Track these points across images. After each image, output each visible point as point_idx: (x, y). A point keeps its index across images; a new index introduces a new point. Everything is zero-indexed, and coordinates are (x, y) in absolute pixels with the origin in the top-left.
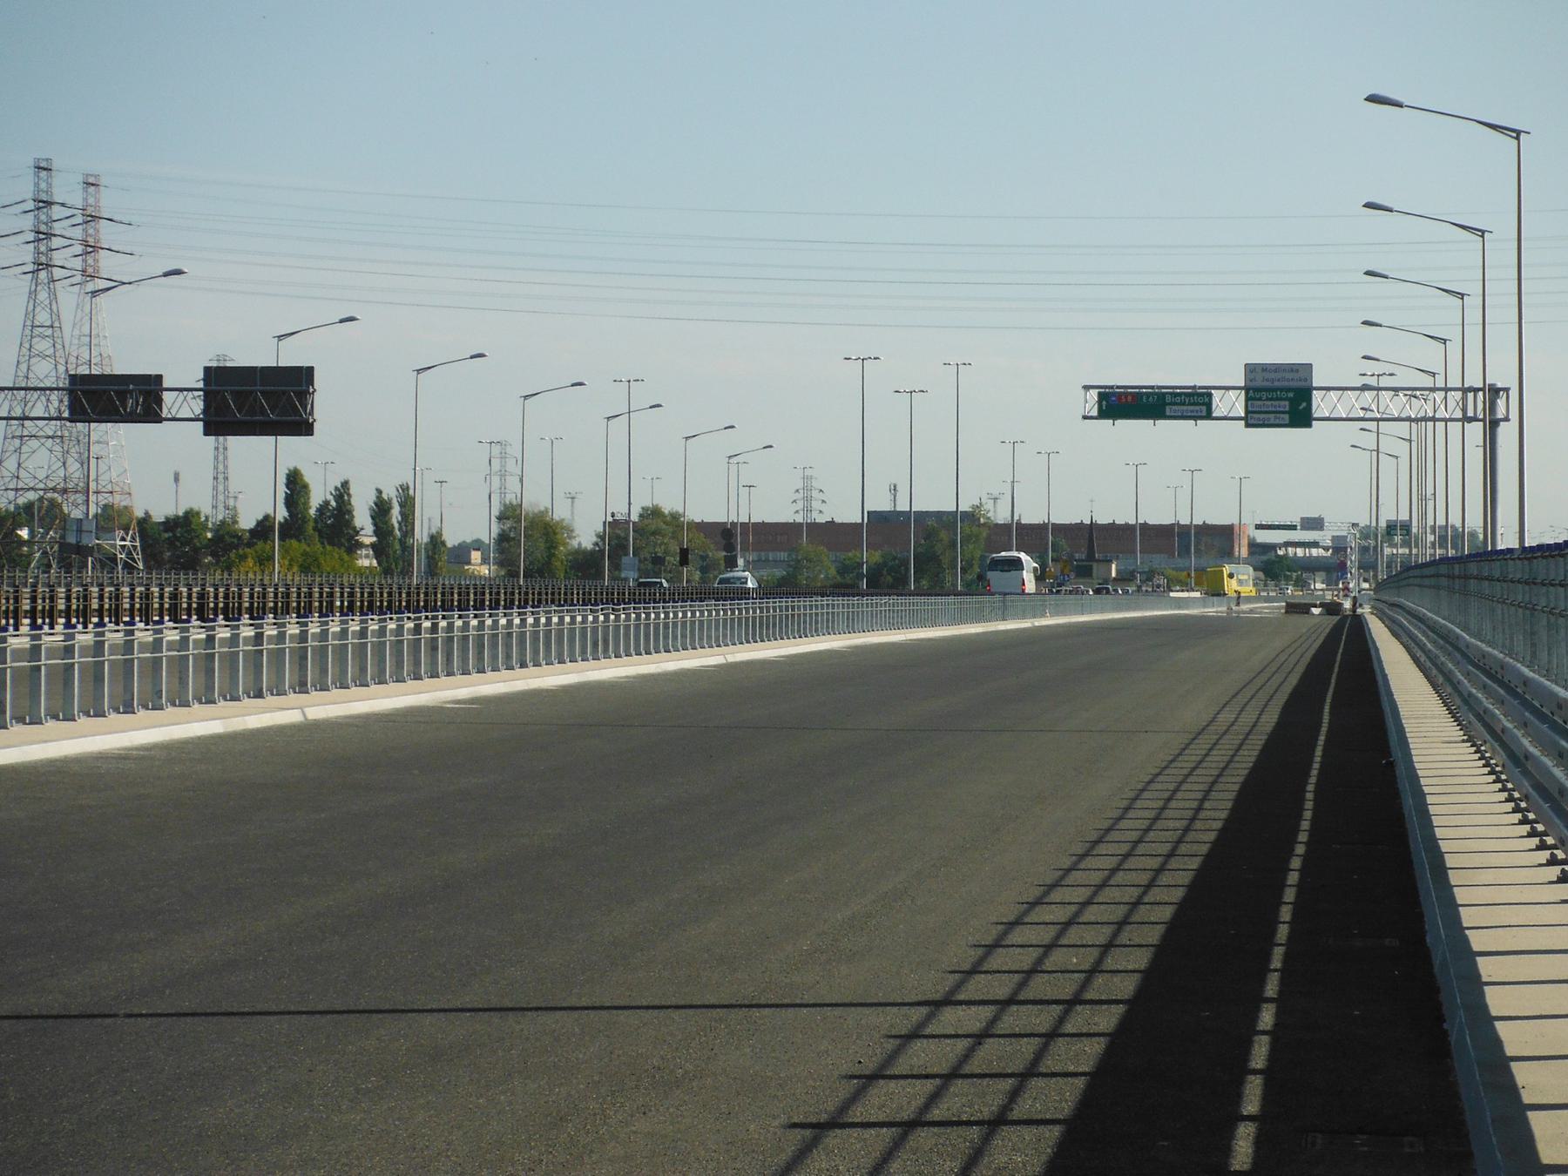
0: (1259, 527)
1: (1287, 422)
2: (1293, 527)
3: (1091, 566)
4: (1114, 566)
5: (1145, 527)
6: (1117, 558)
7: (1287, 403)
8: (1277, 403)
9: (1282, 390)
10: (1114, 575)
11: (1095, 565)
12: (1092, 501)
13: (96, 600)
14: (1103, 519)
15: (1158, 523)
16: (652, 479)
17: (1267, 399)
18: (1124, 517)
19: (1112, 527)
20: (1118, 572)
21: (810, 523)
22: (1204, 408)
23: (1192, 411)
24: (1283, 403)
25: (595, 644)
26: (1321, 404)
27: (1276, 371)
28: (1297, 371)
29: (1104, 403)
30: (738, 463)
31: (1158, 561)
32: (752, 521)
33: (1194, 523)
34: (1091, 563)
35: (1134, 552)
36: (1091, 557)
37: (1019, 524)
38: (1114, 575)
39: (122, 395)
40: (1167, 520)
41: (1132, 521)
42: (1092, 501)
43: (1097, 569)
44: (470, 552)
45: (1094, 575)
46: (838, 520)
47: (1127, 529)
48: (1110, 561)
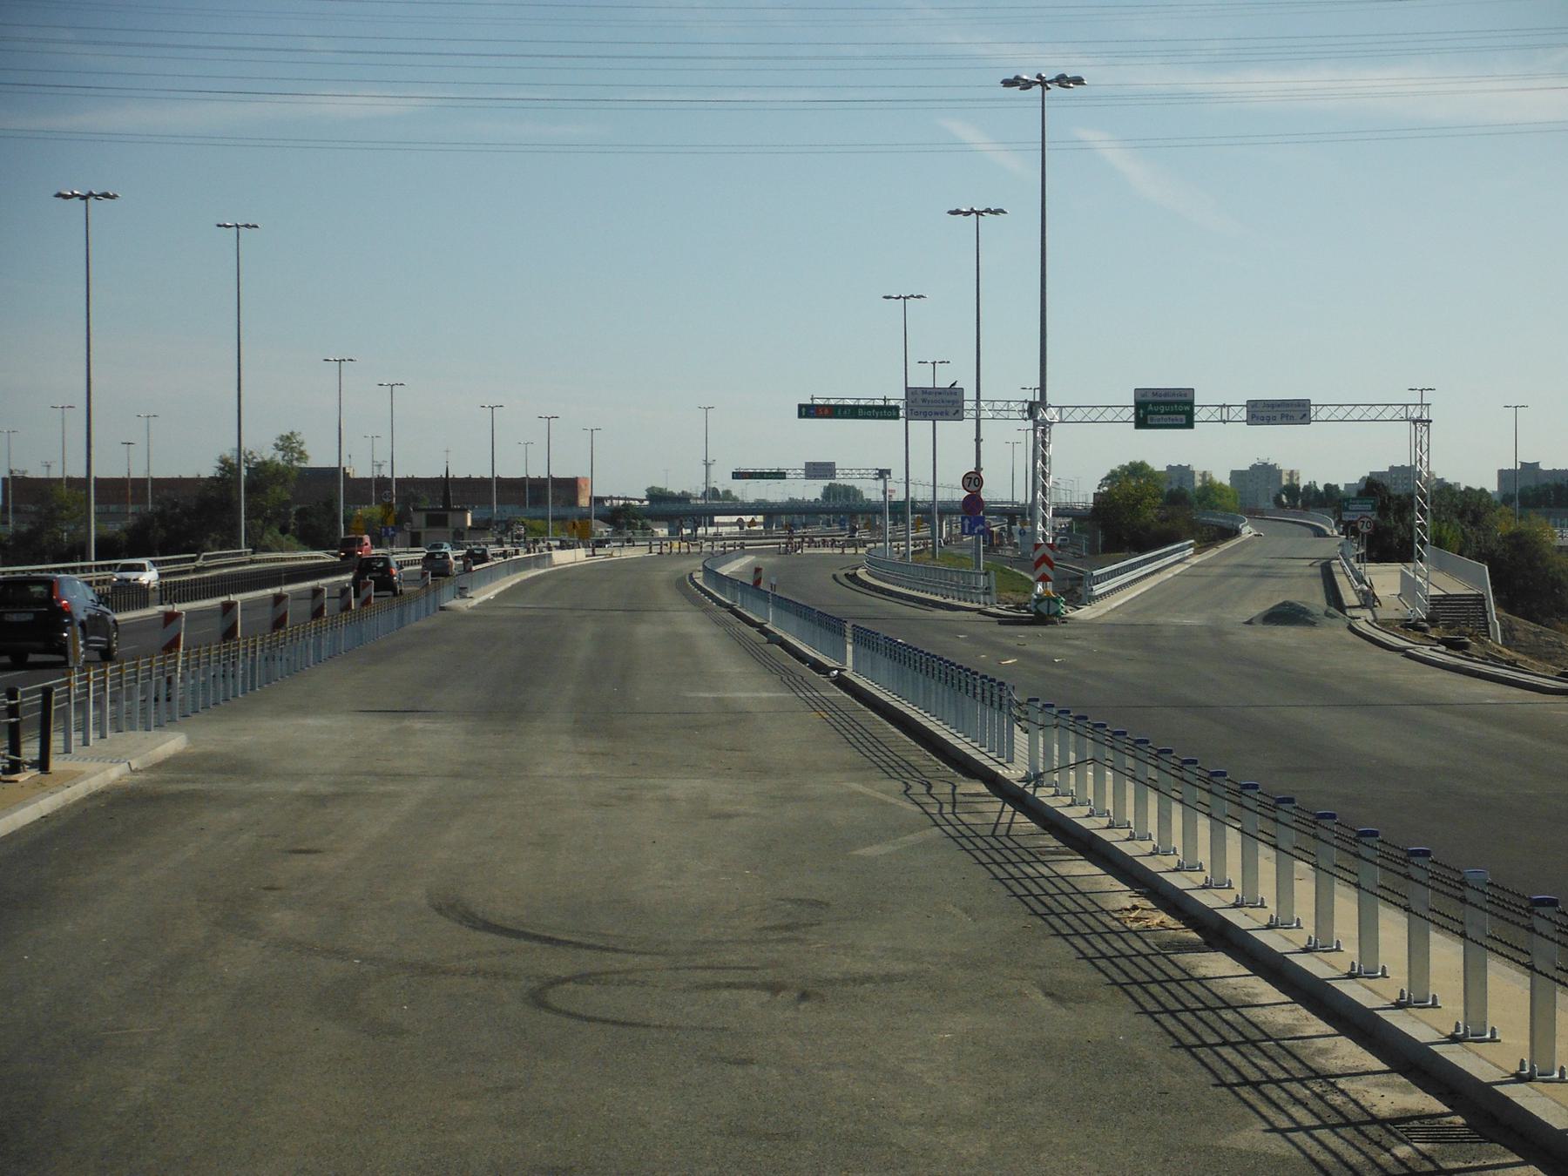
0: (737, 475)
1: (1184, 422)
2: (780, 475)
3: (446, 515)
4: (469, 515)
5: (501, 482)
6: (473, 508)
7: (1370, 506)
8: (1171, 416)
9: (1178, 403)
10: (469, 524)
11: (450, 514)
12: (447, 451)
13: (720, 528)
14: (459, 472)
15: (429, 477)
16: (9, 432)
17: (1165, 413)
18: (481, 471)
19: (469, 481)
20: (473, 520)
21: (806, 474)
22: (1183, 417)
23: (1166, 420)
24: (1179, 417)
25: (120, 606)
26: (1200, 414)
27: (1165, 395)
28: (1185, 395)
29: (1141, 411)
30: (63, 407)
31: (510, 511)
32: (132, 477)
33: (97, 472)
34: (445, 513)
35: (491, 503)
36: (447, 507)
37: (498, 478)
38: (469, 524)
39: (843, 410)
40: (518, 474)
41: (488, 475)
42: (447, 451)
43: (452, 518)
44: (1231, 484)
45: (450, 525)
46: (184, 476)
47: (483, 484)
48: (465, 511)
